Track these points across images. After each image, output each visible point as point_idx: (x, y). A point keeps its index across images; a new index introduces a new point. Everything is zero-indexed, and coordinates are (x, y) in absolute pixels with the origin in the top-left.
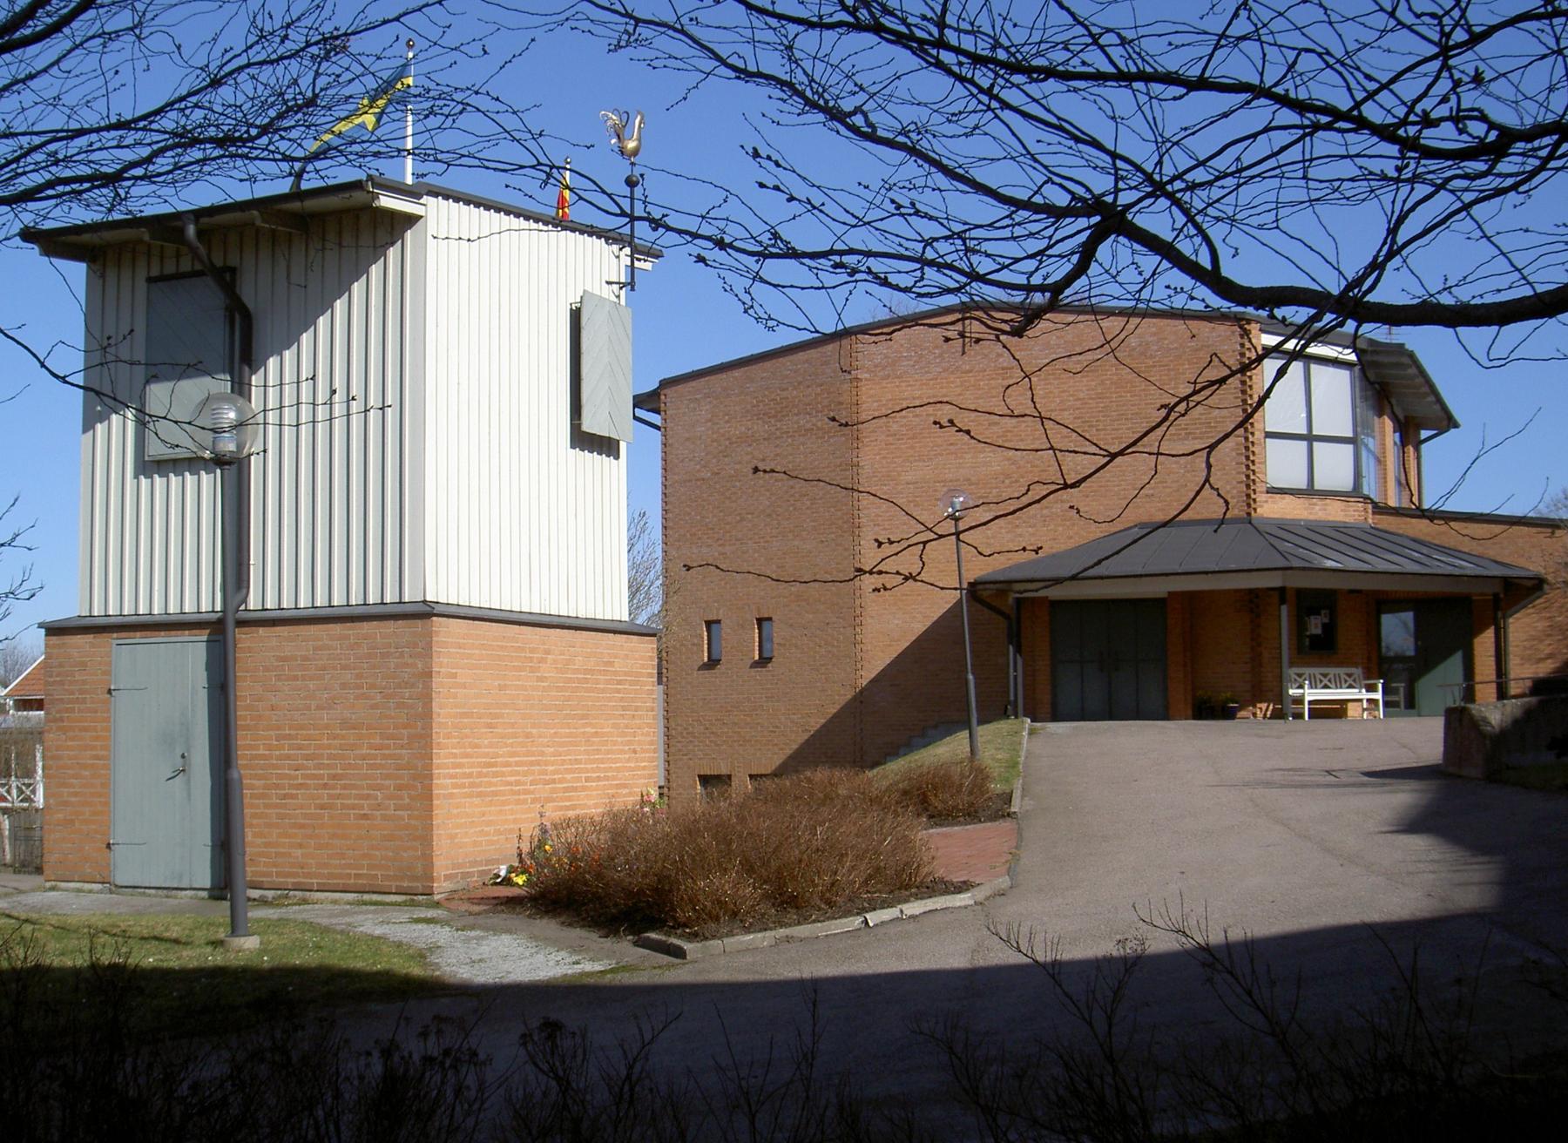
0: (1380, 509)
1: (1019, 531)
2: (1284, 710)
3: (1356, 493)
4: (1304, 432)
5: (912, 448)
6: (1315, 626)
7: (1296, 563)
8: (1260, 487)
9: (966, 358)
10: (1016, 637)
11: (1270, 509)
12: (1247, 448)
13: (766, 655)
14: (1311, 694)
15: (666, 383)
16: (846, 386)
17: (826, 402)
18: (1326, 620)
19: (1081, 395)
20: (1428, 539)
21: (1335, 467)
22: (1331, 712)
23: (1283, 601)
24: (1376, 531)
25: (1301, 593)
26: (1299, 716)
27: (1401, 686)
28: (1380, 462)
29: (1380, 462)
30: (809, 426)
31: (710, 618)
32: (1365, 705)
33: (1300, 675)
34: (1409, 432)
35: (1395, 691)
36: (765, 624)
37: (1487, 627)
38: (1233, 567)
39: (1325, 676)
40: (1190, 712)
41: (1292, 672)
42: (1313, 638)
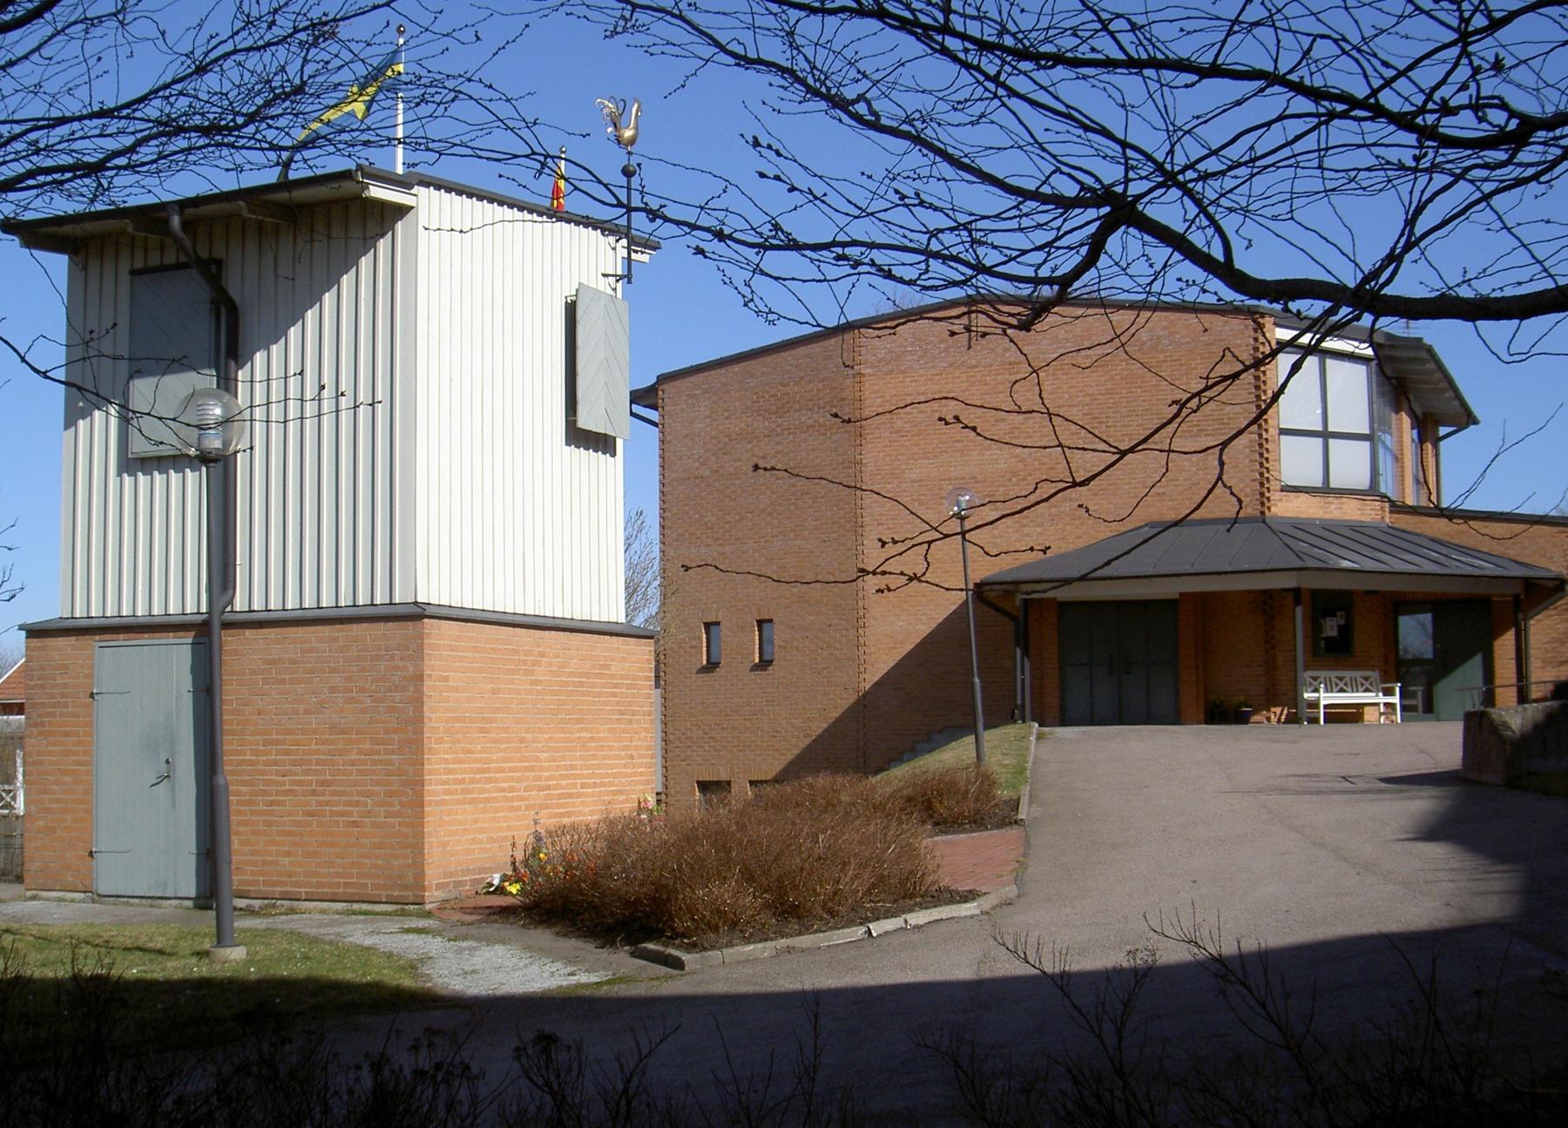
0: (1397, 508)
1: (1027, 530)
2: (1299, 715)
3: (1373, 491)
4: (1319, 428)
5: (917, 445)
6: (1331, 628)
7: (1311, 563)
8: (1274, 485)
10: (1023, 639)
11: (1284, 507)
12: (1261, 445)
13: (713, 660)
14: (1326, 698)
15: (664, 379)
16: (848, 382)
18: (1342, 622)
19: (1091, 391)
20: (1446, 538)
22: (1348, 716)
23: (1297, 602)
24: (1393, 531)
25: (1315, 593)
26: (1314, 720)
27: (1419, 690)
28: (1398, 459)
29: (1398, 459)
30: (810, 422)
33: (1315, 679)
34: (1427, 429)
35: (1413, 695)
37: (1506, 629)
38: (1246, 567)
39: (1341, 679)
40: (1202, 717)
41: (1307, 675)
42: (1327, 639)
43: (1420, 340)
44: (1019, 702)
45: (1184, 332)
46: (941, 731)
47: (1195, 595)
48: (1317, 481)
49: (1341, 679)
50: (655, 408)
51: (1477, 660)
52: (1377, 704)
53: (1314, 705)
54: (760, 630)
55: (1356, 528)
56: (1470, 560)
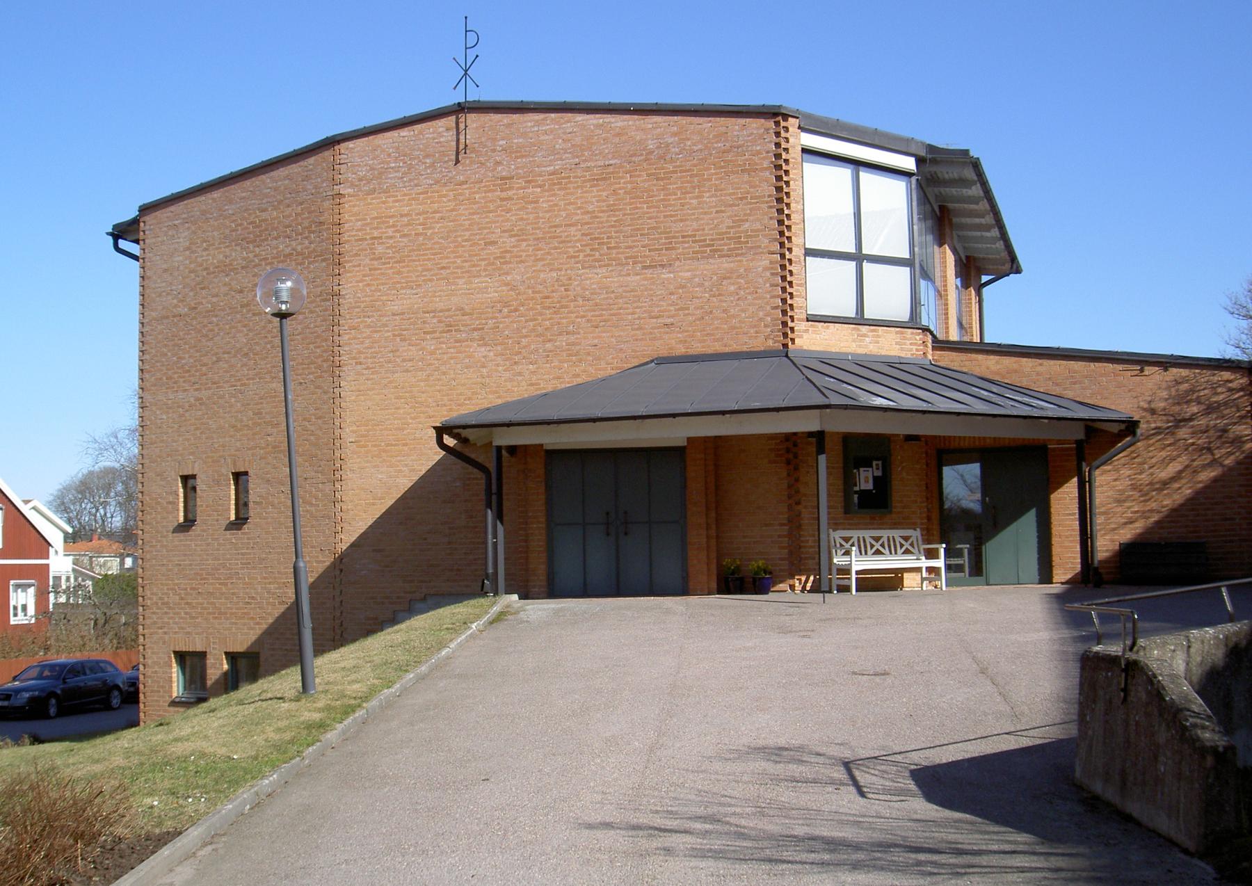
0: (941, 345)
1: (518, 368)
2: (828, 583)
3: (913, 323)
4: (851, 249)
5: (399, 273)
6: (865, 480)
7: (835, 400)
8: (799, 314)
9: (460, 167)
10: (495, 498)
11: (809, 340)
12: (783, 267)
13: (190, 516)
14: (859, 563)
15: (145, 209)
16: (327, 204)
17: (306, 223)
18: (879, 473)
19: (590, 208)
20: (997, 378)
21: (889, 292)
22: (886, 583)
23: (821, 450)
24: (935, 368)
25: (848, 440)
26: (845, 589)
27: (965, 547)
28: (941, 295)
29: (941, 295)
30: (288, 251)
31: (186, 473)
32: (925, 574)
33: (847, 540)
34: (973, 271)
35: (959, 554)
36: (191, 482)
37: (1067, 480)
38: (757, 405)
39: (877, 539)
40: (714, 585)
41: (837, 535)
42: (862, 493)
43: (966, 152)
44: (490, 571)
45: (696, 138)
46: (424, 599)
47: (706, 440)
48: (851, 313)
49: (877, 539)
50: (137, 242)
51: (1030, 517)
52: (918, 570)
53: (845, 571)
54: (236, 484)
55: (895, 365)
56: (1026, 399)
